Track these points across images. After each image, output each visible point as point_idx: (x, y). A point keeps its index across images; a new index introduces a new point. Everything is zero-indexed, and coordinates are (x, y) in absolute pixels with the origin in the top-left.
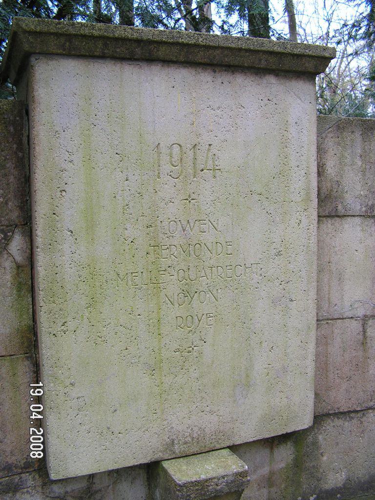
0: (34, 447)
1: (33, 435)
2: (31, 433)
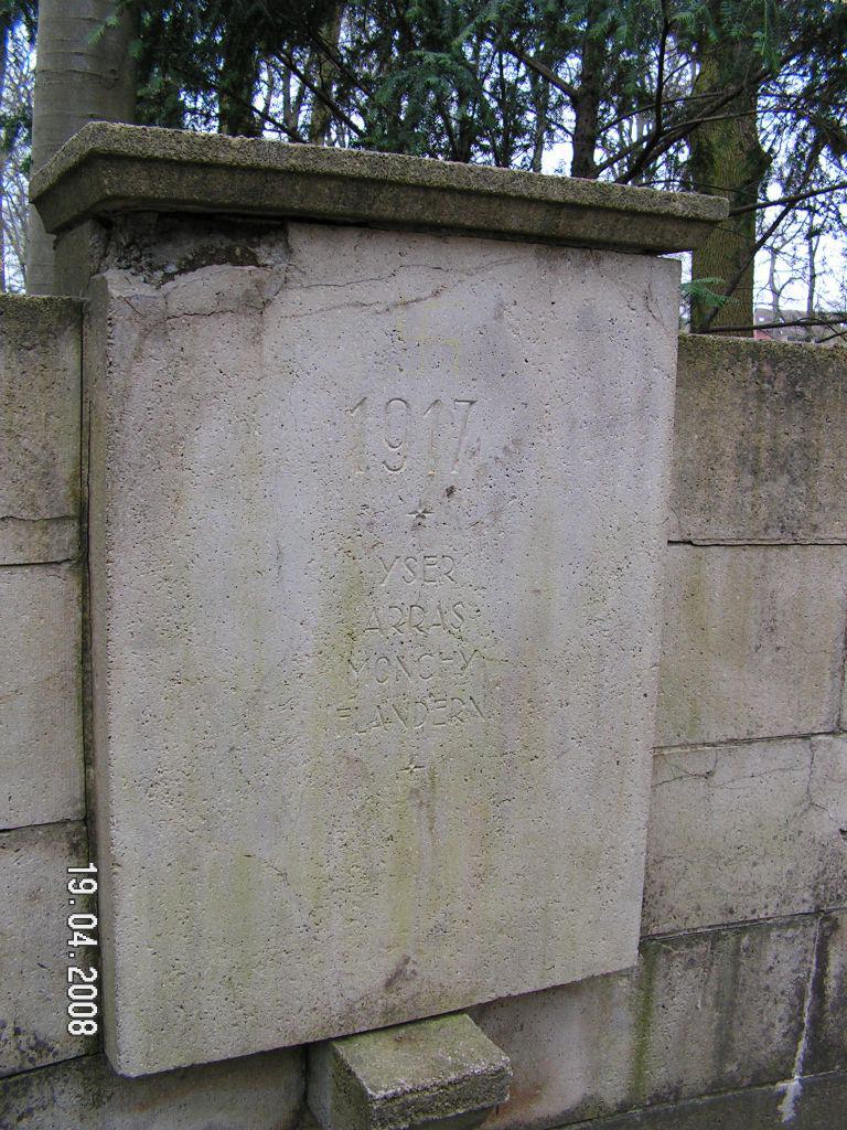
1: (73, 983)
2: (70, 979)
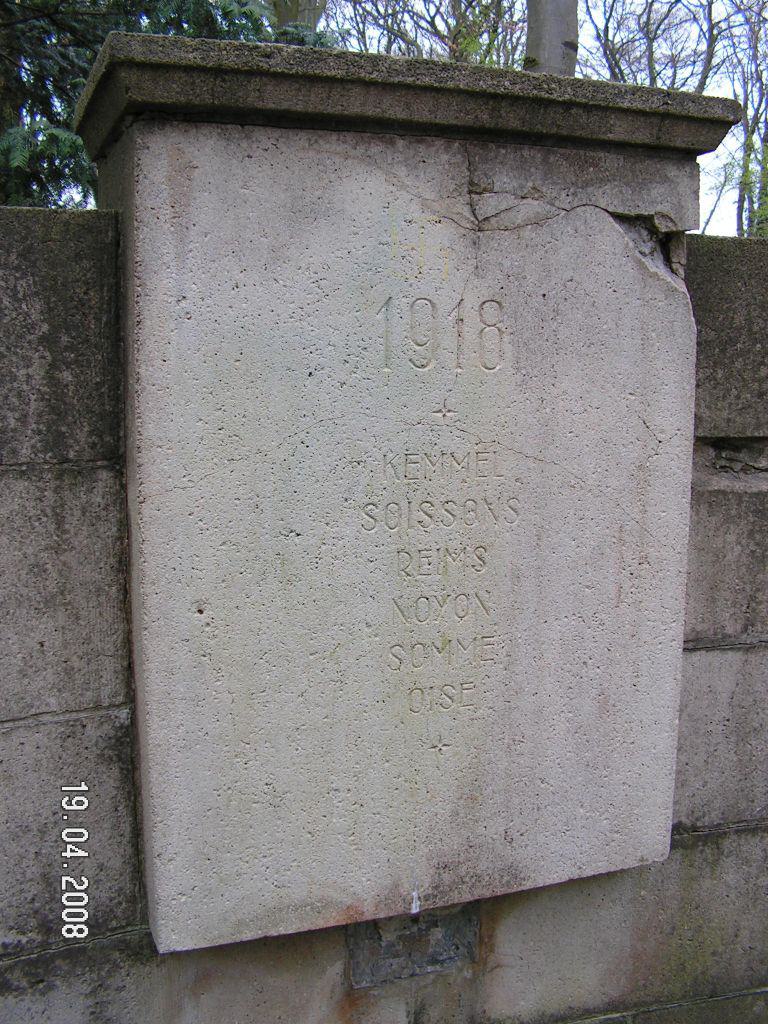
0: (70, 915)
1: (66, 891)
2: (64, 887)
